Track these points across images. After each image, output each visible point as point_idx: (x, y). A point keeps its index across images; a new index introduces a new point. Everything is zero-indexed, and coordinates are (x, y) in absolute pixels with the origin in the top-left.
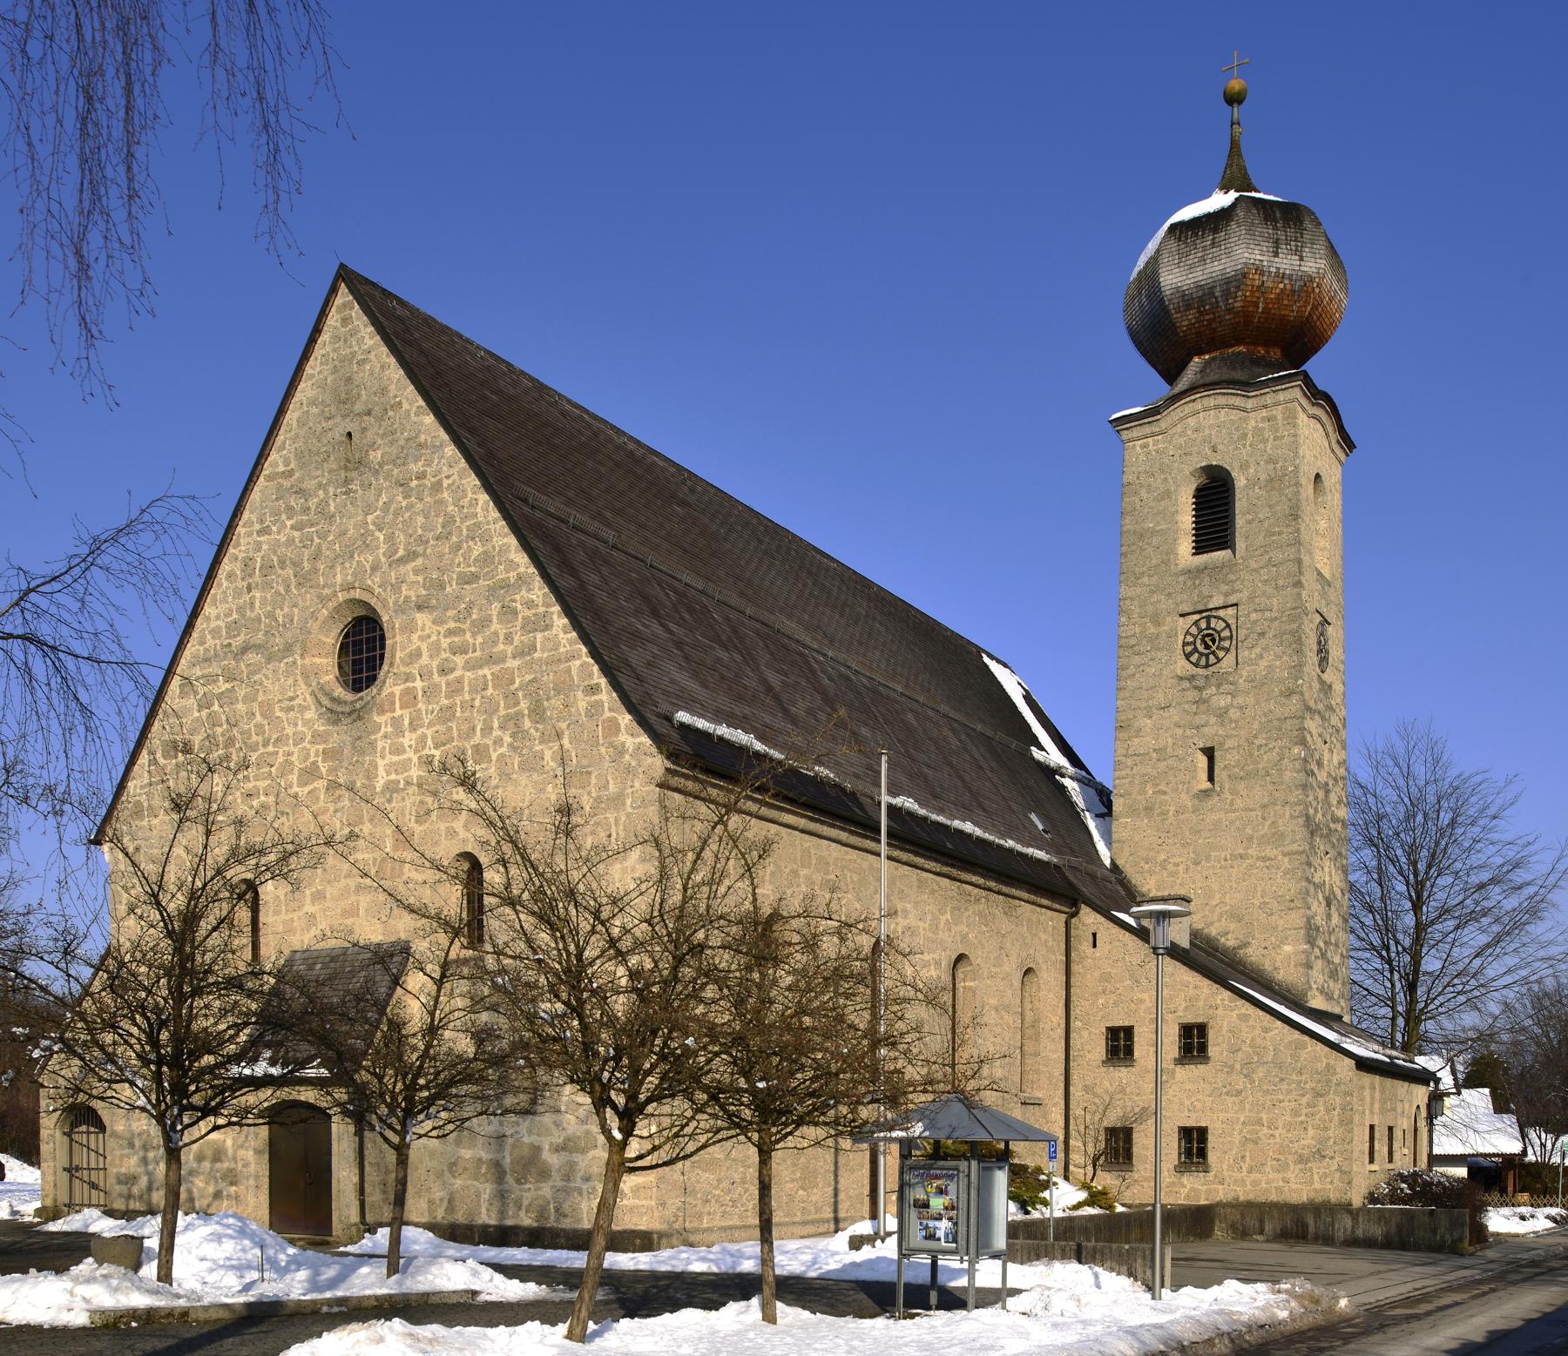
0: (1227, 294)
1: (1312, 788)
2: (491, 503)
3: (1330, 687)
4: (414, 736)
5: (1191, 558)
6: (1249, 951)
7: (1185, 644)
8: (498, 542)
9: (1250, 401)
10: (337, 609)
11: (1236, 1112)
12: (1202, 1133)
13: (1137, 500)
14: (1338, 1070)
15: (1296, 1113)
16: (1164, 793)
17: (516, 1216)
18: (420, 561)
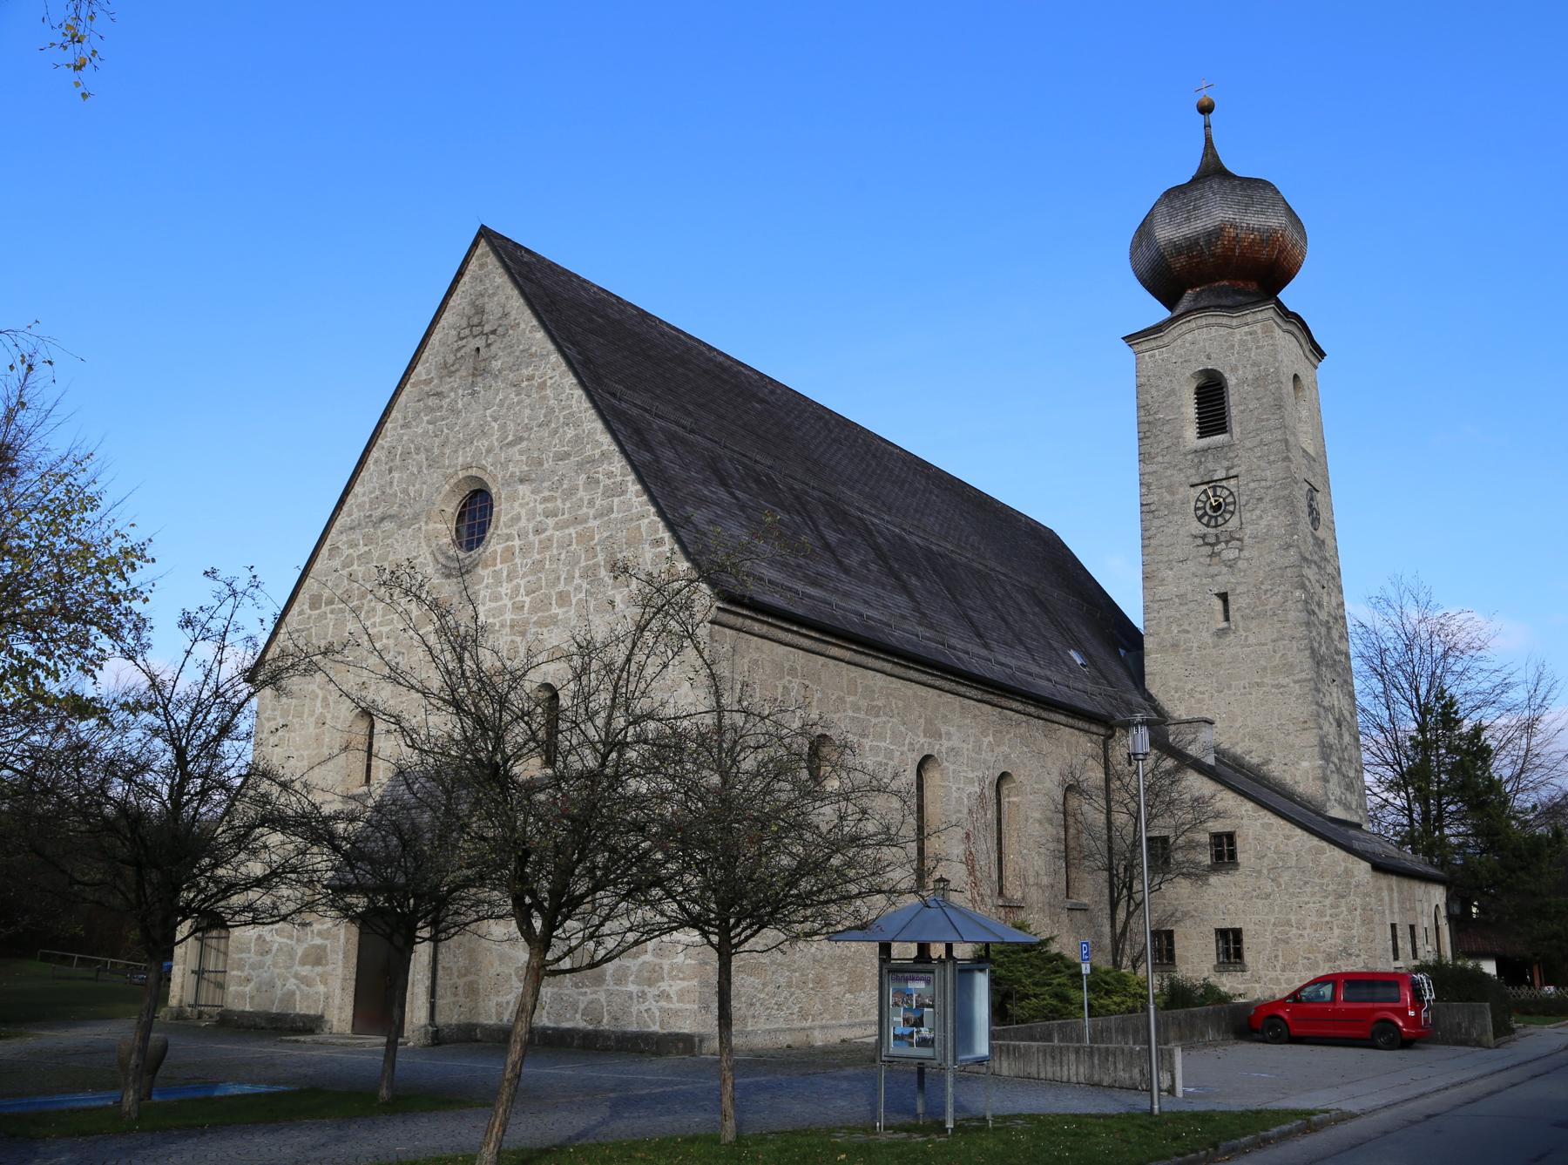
0: (1209, 243)
1: (1315, 625)
2: (584, 397)
3: (1323, 542)
4: (510, 586)
5: (1197, 441)
6: (1271, 767)
7: (1197, 509)
8: (587, 426)
9: (1235, 320)
10: (457, 485)
11: (1267, 914)
12: (1237, 933)
13: (1149, 397)
14: (1356, 873)
15: (1321, 914)
16: (1188, 632)
17: (573, 1019)
18: (525, 443)
